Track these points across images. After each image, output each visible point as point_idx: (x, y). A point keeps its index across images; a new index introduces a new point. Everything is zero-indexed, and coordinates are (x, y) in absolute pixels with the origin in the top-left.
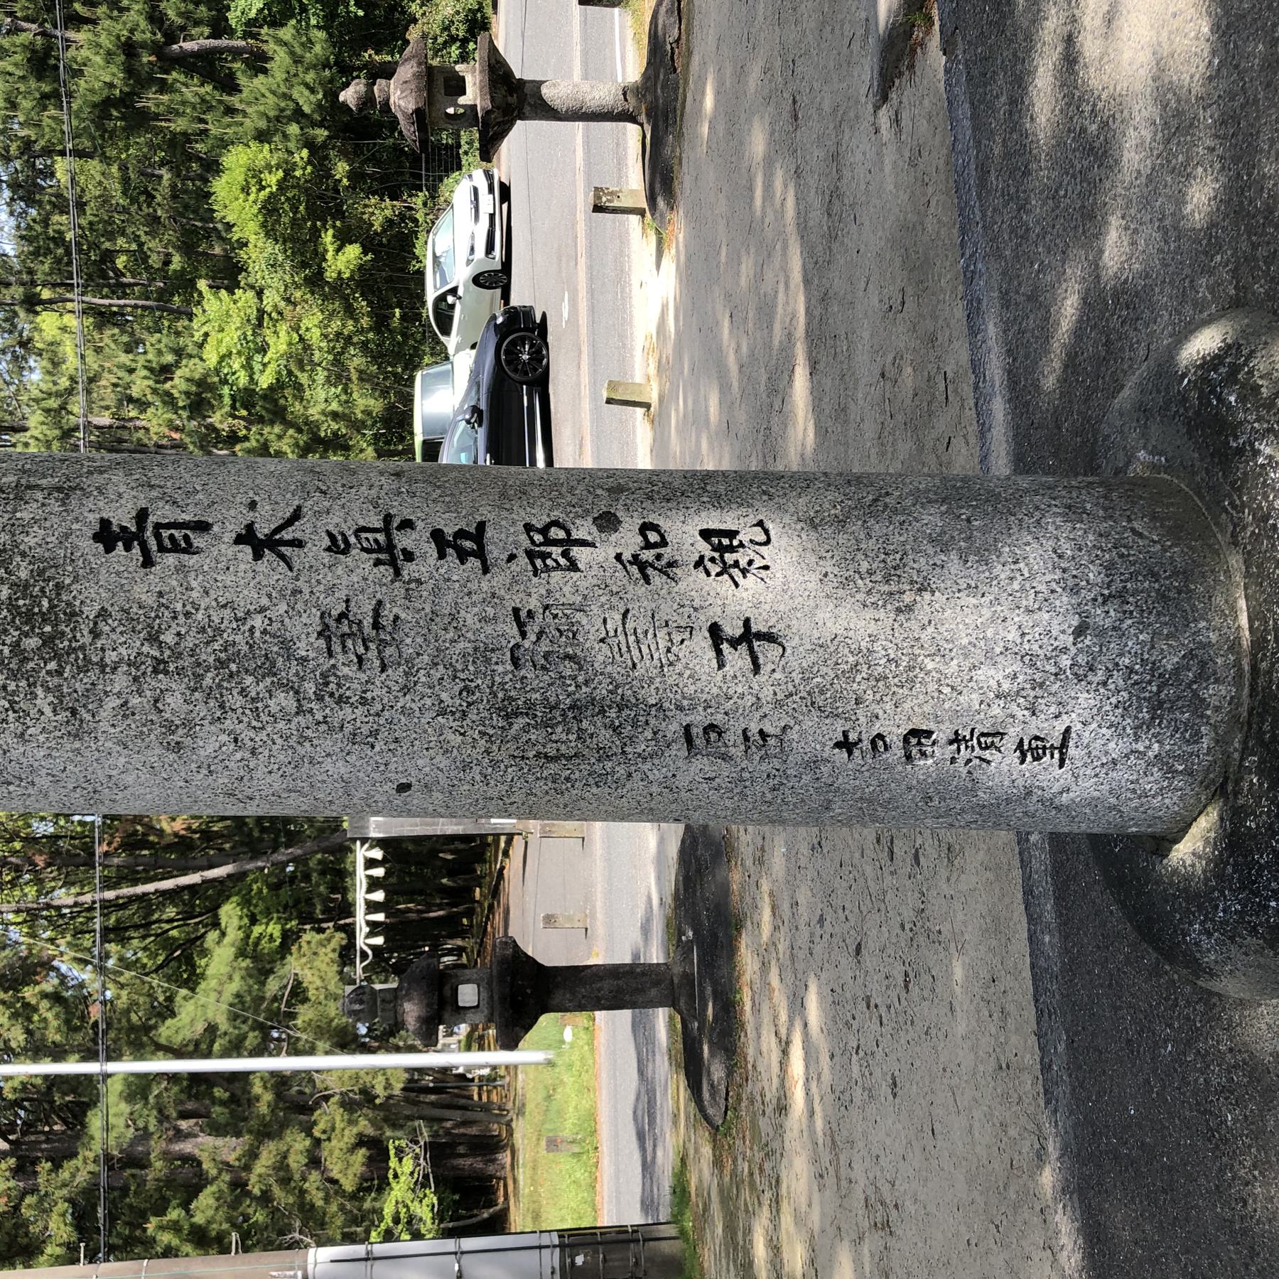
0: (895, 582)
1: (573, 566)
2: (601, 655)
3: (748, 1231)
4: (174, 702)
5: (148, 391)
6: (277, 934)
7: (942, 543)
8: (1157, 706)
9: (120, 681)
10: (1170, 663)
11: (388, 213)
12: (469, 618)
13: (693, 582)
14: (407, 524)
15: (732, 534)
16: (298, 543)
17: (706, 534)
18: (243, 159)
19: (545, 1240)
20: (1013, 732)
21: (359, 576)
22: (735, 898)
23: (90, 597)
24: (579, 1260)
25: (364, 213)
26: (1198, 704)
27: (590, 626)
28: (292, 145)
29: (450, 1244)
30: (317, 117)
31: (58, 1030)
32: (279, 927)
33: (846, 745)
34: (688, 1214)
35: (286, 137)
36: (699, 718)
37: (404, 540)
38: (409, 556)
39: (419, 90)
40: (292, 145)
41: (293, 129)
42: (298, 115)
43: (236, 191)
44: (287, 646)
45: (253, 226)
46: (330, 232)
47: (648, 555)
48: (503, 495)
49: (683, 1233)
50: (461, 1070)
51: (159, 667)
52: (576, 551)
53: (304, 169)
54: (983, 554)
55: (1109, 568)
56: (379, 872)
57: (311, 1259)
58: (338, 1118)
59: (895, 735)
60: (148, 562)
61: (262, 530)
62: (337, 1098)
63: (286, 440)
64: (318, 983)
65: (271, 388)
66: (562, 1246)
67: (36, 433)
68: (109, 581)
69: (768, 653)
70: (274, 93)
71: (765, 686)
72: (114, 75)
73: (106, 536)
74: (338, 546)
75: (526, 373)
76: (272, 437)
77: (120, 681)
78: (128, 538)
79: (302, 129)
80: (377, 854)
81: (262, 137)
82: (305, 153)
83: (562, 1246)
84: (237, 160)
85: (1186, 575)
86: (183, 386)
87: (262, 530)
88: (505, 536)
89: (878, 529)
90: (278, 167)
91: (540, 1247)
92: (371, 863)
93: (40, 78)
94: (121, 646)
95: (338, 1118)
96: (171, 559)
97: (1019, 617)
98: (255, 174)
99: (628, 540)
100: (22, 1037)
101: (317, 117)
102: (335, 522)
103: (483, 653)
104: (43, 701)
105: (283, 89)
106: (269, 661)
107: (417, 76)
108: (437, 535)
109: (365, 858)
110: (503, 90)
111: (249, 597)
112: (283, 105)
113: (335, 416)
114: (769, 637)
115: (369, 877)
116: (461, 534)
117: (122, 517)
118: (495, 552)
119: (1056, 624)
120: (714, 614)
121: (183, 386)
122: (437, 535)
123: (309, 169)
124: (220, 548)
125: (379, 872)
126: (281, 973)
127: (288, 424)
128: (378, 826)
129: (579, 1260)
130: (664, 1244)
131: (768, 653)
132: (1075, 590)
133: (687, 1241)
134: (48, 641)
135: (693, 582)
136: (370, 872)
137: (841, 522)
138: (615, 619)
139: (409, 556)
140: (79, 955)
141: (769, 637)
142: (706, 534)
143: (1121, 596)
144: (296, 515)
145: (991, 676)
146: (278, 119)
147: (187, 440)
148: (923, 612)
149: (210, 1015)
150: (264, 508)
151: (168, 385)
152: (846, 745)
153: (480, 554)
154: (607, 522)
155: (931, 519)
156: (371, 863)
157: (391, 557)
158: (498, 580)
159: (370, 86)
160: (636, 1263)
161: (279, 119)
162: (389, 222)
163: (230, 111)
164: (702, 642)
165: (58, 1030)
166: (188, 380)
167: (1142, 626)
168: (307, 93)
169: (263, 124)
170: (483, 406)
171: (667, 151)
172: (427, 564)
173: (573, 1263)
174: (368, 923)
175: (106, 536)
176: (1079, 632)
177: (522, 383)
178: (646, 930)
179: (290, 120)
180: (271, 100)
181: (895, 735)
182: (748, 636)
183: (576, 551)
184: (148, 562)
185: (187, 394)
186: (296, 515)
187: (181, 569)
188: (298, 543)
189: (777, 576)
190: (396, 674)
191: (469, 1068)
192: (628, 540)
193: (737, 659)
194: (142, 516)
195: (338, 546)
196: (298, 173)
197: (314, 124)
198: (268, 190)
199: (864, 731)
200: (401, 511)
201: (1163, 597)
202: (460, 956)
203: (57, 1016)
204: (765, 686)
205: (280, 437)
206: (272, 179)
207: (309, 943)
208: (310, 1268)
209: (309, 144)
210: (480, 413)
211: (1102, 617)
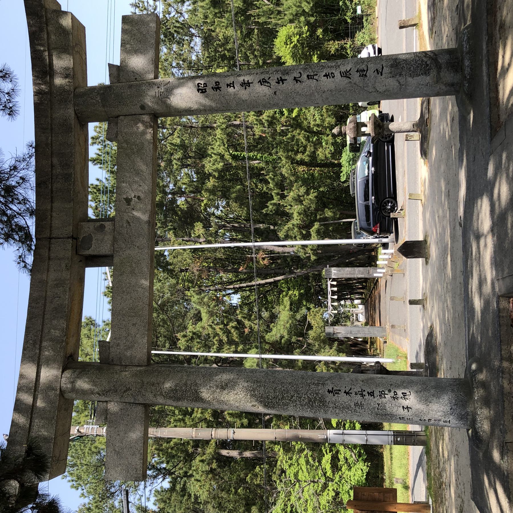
0: (427, 401)
1: (385, 398)
2: (388, 409)
3: (439, 443)
4: (337, 411)
5: (255, 120)
6: (297, 294)
7: (433, 396)
8: (461, 418)
9: (331, 409)
10: (463, 413)
11: (337, 46)
12: (372, 404)
13: (400, 400)
14: (364, 391)
15: (406, 393)
16: (351, 393)
17: (402, 393)
18: (285, 33)
19: (390, 433)
20: (442, 420)
21: (359, 398)
22: (437, 363)
23: (328, 399)
24: (399, 439)
25: (328, 48)
26: (467, 419)
27: (387, 406)
28: (302, 25)
29: (364, 432)
30: (310, 13)
31: (237, 338)
32: (298, 292)
33: (420, 420)
34: (428, 431)
35: (299, 22)
36: (401, 417)
37: (364, 393)
38: (365, 395)
39: (354, 132)
40: (302, 25)
41: (302, 19)
42: (304, 13)
43: (283, 43)
44: (350, 406)
45: (288, 57)
46: (316, 56)
47: (395, 396)
48: (376, 386)
49: (426, 435)
50: (365, 363)
51: (336, 408)
52: (386, 395)
53: (306, 33)
54: (438, 398)
55: (456, 400)
56: (335, 289)
57: (328, 433)
58: (324, 369)
59: (427, 419)
60: (334, 395)
61: (347, 391)
62: (323, 362)
63: (301, 135)
64: (316, 325)
65: (296, 116)
66: (394, 435)
67: (219, 137)
68: (330, 397)
69: (410, 410)
70: (295, 5)
71: (410, 413)
72: (239, 4)
73: (329, 391)
74: (356, 394)
75: (386, 138)
76: (296, 134)
77: (331, 409)
78: (332, 392)
79: (305, 18)
80: (335, 283)
81: (291, 21)
82: (307, 27)
83: (394, 435)
84: (283, 33)
85: (466, 402)
86: (266, 118)
87: (347, 391)
88: (377, 393)
89: (425, 393)
90: (297, 34)
91: (388, 435)
92: (332, 286)
93: (214, 7)
94: (331, 405)
95: (324, 369)
96: (337, 395)
97: (443, 407)
98: (289, 37)
99: (392, 394)
100: (226, 339)
101: (310, 13)
102: (355, 390)
103: (374, 408)
104: (322, 410)
105: (298, 4)
106: (348, 408)
107: (354, 127)
108: (368, 392)
109: (331, 284)
110: (378, 129)
111: (346, 400)
112: (298, 9)
113: (318, 125)
114: (410, 408)
115: (332, 291)
116: (371, 392)
117: (330, 389)
118: (375, 395)
119: (448, 408)
120: (403, 405)
121: (266, 118)
122: (368, 392)
123: (308, 33)
124: (342, 394)
125: (335, 289)
126: (300, 312)
127: (302, 128)
128: (335, 274)
129: (399, 439)
130: (422, 437)
131: (410, 410)
132: (451, 403)
133: (427, 437)
134: (323, 404)
135: (400, 400)
136: (333, 297)
137: (421, 392)
138: (390, 405)
139: (365, 395)
140: (243, 316)
141: (410, 408)
142: (402, 393)
143: (457, 404)
144: (351, 389)
145: (439, 414)
146: (296, 15)
147: (268, 135)
148: (430, 406)
149: (282, 333)
150: (347, 388)
151: (261, 118)
152: (420, 420)
153: (373, 395)
154: (390, 391)
155: (433, 391)
156: (332, 286)
157: (363, 396)
158: (376, 399)
159: (341, 128)
160: (414, 441)
161: (297, 15)
162: (337, 50)
163: (279, 12)
164: (401, 408)
165: (237, 338)
166: (268, 116)
167: (459, 409)
168: (306, 4)
169: (291, 17)
170: (371, 151)
171: (425, 146)
172: (367, 397)
173: (397, 440)
174: (331, 298)
175: (329, 391)
176: (451, 409)
177: (385, 142)
178: (420, 346)
179: (301, 15)
180: (295, 8)
181: (427, 419)
182: (407, 407)
183: (386, 395)
184: (334, 395)
185: (267, 121)
186: (351, 389)
187: (338, 396)
188: (351, 393)
189: (411, 400)
190: (363, 410)
191: (367, 363)
192: (392, 394)
193: (406, 410)
194: (333, 388)
195: (356, 394)
196: (304, 36)
197: (309, 15)
198: (294, 43)
199: (422, 418)
200: (364, 389)
201: (463, 405)
202: (362, 295)
203: (236, 333)
204: (410, 413)
205: (299, 134)
206: (295, 39)
207: (313, 311)
208: (328, 435)
209: (308, 23)
210: (370, 153)
211: (454, 407)
